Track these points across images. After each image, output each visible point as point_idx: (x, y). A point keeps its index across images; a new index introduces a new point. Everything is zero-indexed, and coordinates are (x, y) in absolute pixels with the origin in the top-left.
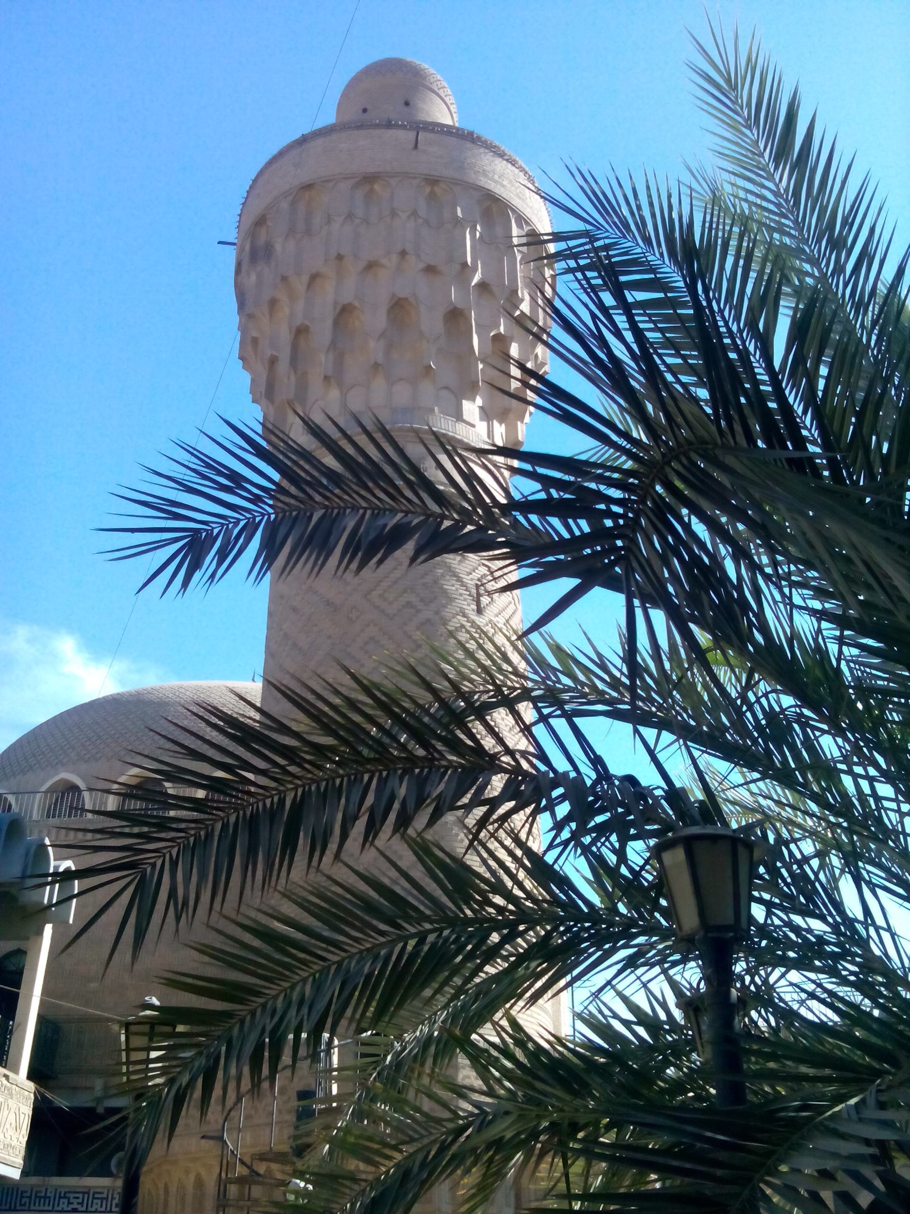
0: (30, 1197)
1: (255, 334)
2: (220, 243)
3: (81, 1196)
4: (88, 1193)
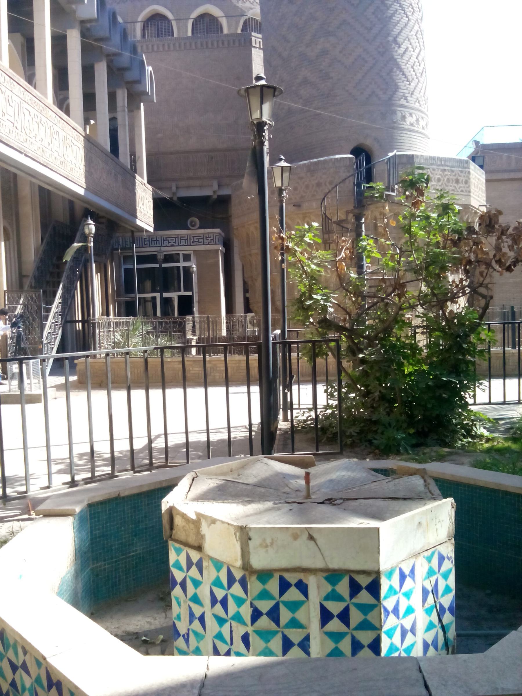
0: (149, 241)
3: (174, 239)
4: (178, 237)
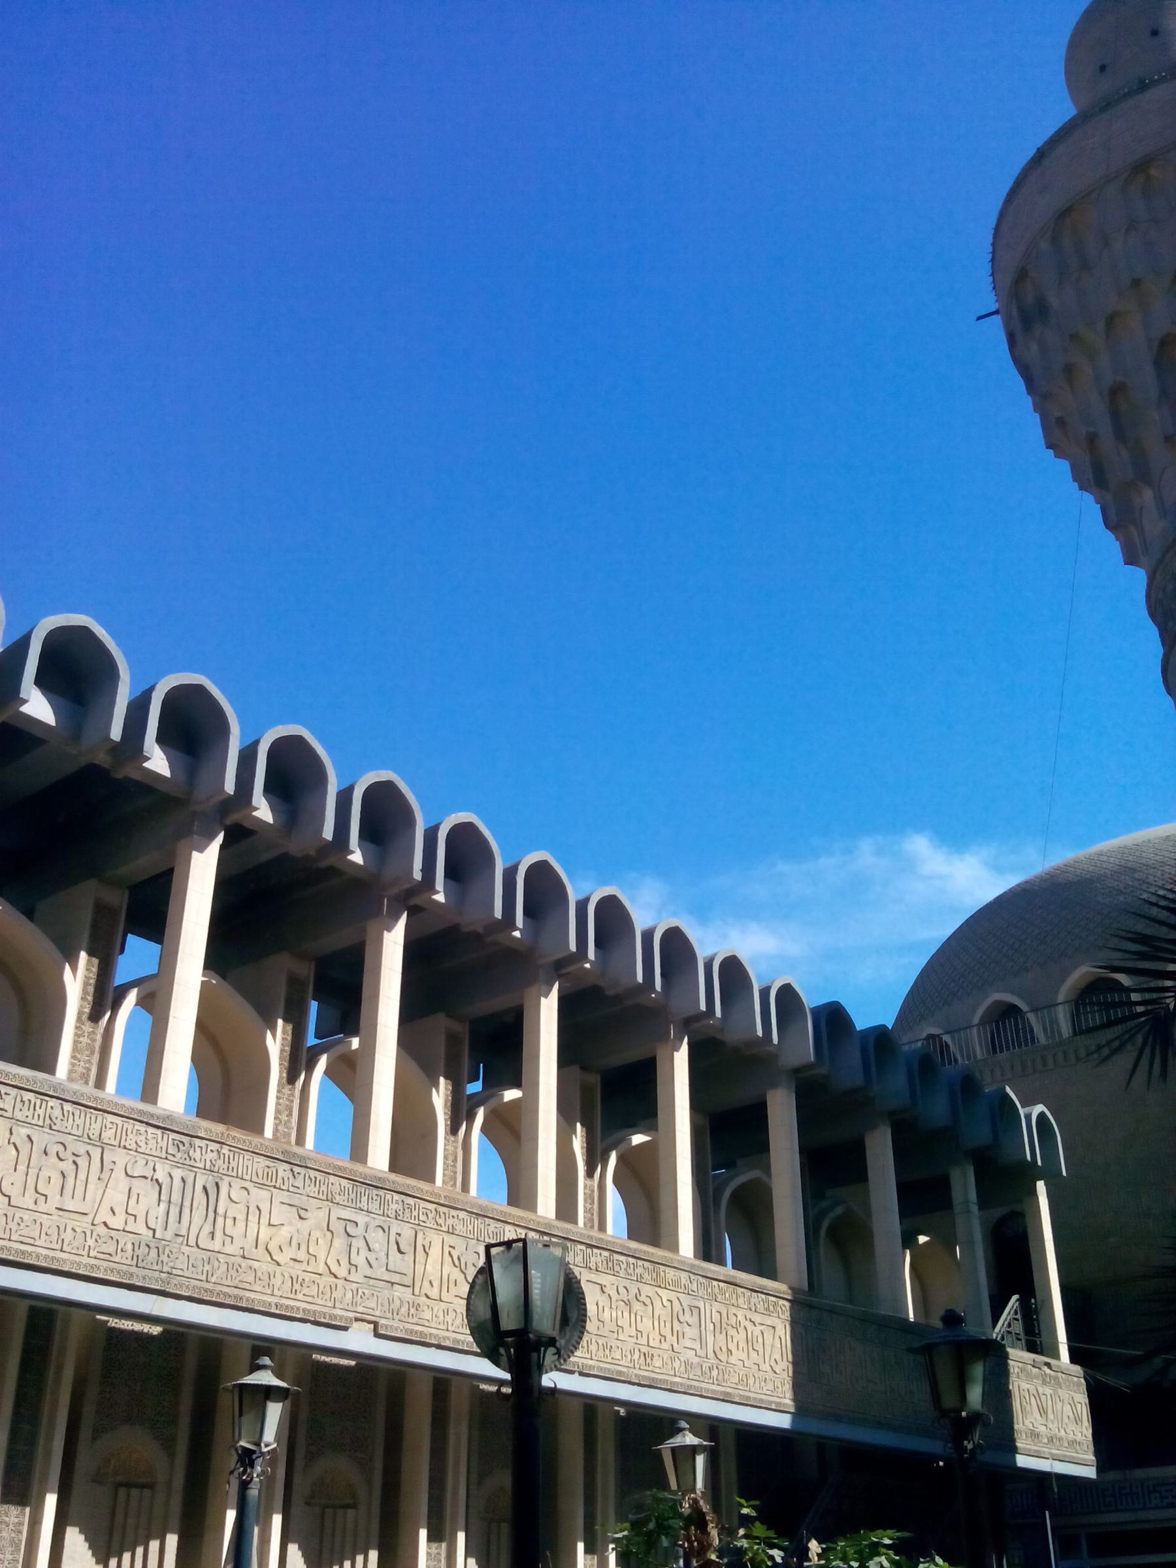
1: (1057, 414)
2: (979, 318)
